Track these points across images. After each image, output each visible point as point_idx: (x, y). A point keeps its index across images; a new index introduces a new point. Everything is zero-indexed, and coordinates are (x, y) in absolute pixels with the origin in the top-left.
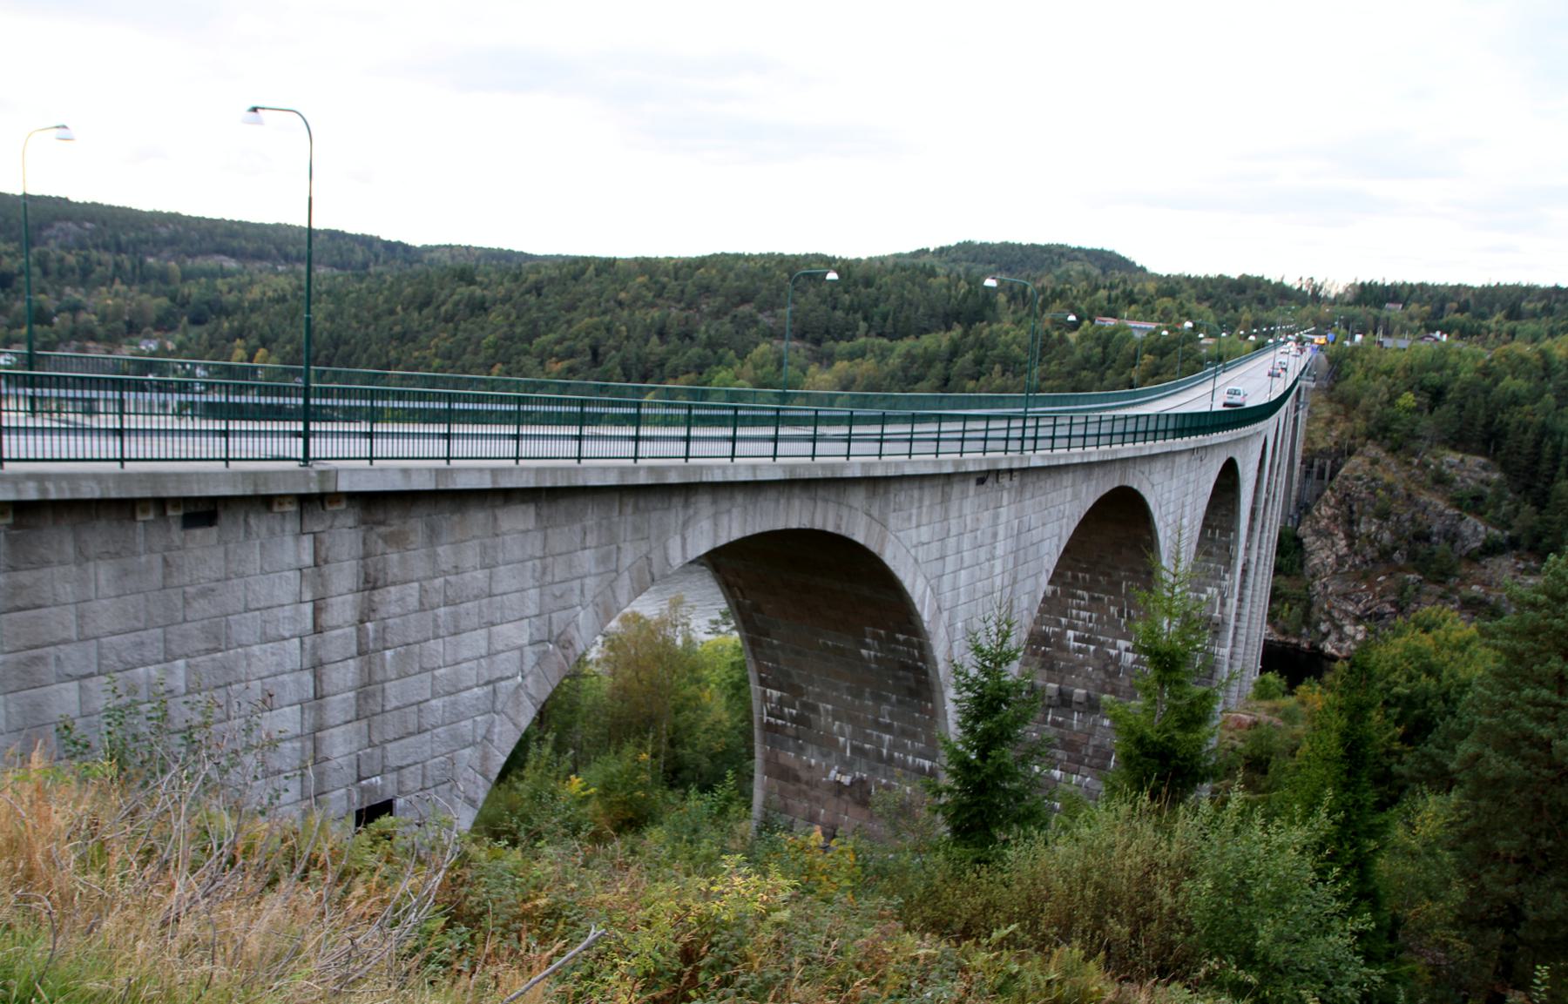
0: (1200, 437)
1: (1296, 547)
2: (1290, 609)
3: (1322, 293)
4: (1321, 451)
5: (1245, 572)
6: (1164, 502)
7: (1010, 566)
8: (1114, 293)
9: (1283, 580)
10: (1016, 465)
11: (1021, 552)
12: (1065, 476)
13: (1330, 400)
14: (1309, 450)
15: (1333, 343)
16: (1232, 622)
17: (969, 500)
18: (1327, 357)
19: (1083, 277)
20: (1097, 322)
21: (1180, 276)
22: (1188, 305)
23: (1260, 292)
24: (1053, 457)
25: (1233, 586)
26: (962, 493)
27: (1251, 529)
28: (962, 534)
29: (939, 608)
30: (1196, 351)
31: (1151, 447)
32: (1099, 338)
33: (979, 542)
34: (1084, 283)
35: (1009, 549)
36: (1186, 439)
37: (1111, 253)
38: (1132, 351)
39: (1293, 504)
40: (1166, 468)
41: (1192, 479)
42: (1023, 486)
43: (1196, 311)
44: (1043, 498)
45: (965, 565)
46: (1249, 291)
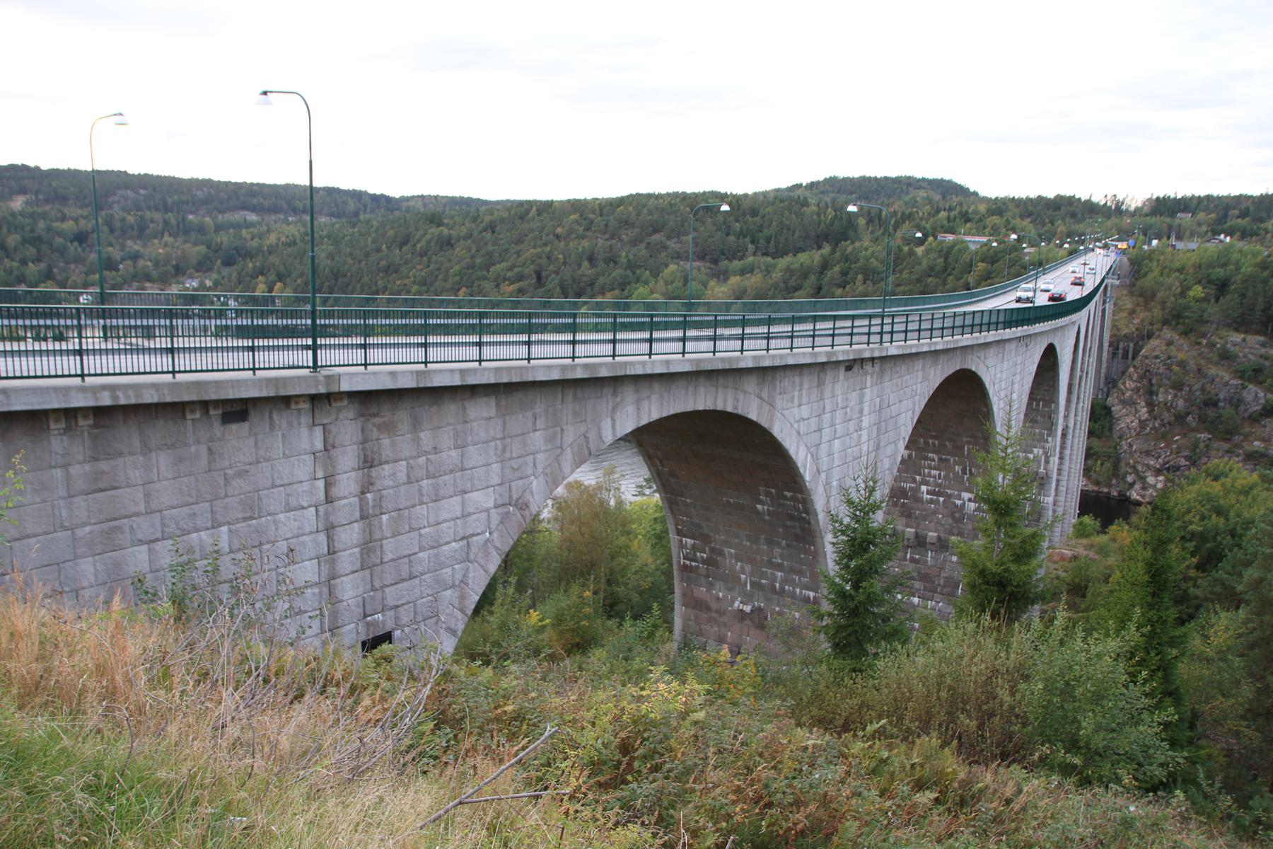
0: (1025, 327)
1: (1106, 414)
2: (1102, 464)
3: (1124, 207)
4: (1125, 336)
5: (1064, 435)
6: (997, 381)
7: (874, 435)
8: (952, 214)
9: (1095, 441)
10: (876, 354)
12: (916, 362)
13: (1132, 294)
14: (1115, 335)
15: (1134, 247)
16: (1055, 476)
18: (1129, 259)
21: (1006, 198)
22: (1013, 221)
23: (1072, 209)
26: (834, 378)
27: (1068, 401)
29: (818, 470)
30: (1020, 259)
31: (985, 336)
32: (941, 251)
33: (848, 417)
34: (928, 207)
35: (873, 422)
36: (1014, 329)
37: (949, 182)
38: (968, 260)
39: (1102, 379)
41: (1019, 362)
42: (882, 371)
44: (899, 380)
45: (838, 435)
46: (1063, 208)
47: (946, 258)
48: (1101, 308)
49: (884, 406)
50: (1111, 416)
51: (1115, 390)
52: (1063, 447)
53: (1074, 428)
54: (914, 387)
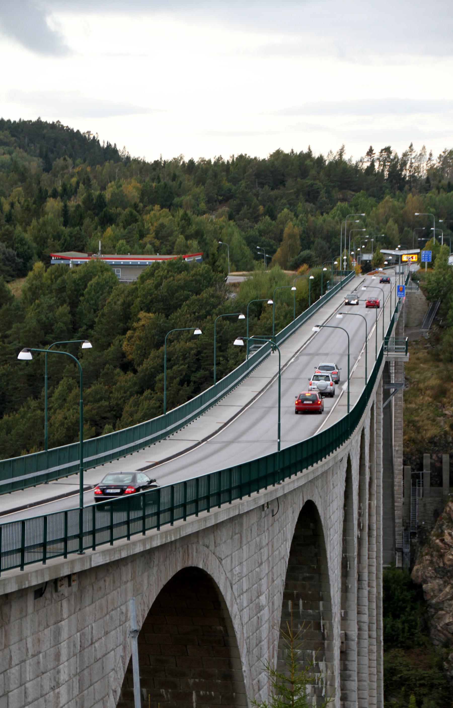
0: (270, 488)
3: (406, 173)
4: (432, 441)
5: (344, 653)
8: (72, 203)
9: (398, 652)
11: (86, 672)
12: (124, 569)
14: (414, 441)
15: (431, 265)
17: (29, 618)
18: (425, 290)
19: (14, 176)
20: (53, 261)
21: (176, 161)
23: (308, 181)
24: (114, 550)
25: (333, 678)
26: (21, 611)
27: (345, 589)
28: (24, 661)
30: (220, 300)
31: (216, 515)
32: (62, 289)
33: (42, 669)
35: (73, 672)
36: (254, 494)
38: (118, 307)
39: (399, 529)
40: (234, 534)
41: (264, 543)
42: (81, 590)
43: (210, 228)
44: (103, 601)
45: (29, 699)
46: (289, 182)
47: (74, 304)
48: (382, 406)
49: (87, 644)
50: (424, 602)
51: (425, 550)
52: (344, 677)
53: (359, 637)
54: (123, 608)
